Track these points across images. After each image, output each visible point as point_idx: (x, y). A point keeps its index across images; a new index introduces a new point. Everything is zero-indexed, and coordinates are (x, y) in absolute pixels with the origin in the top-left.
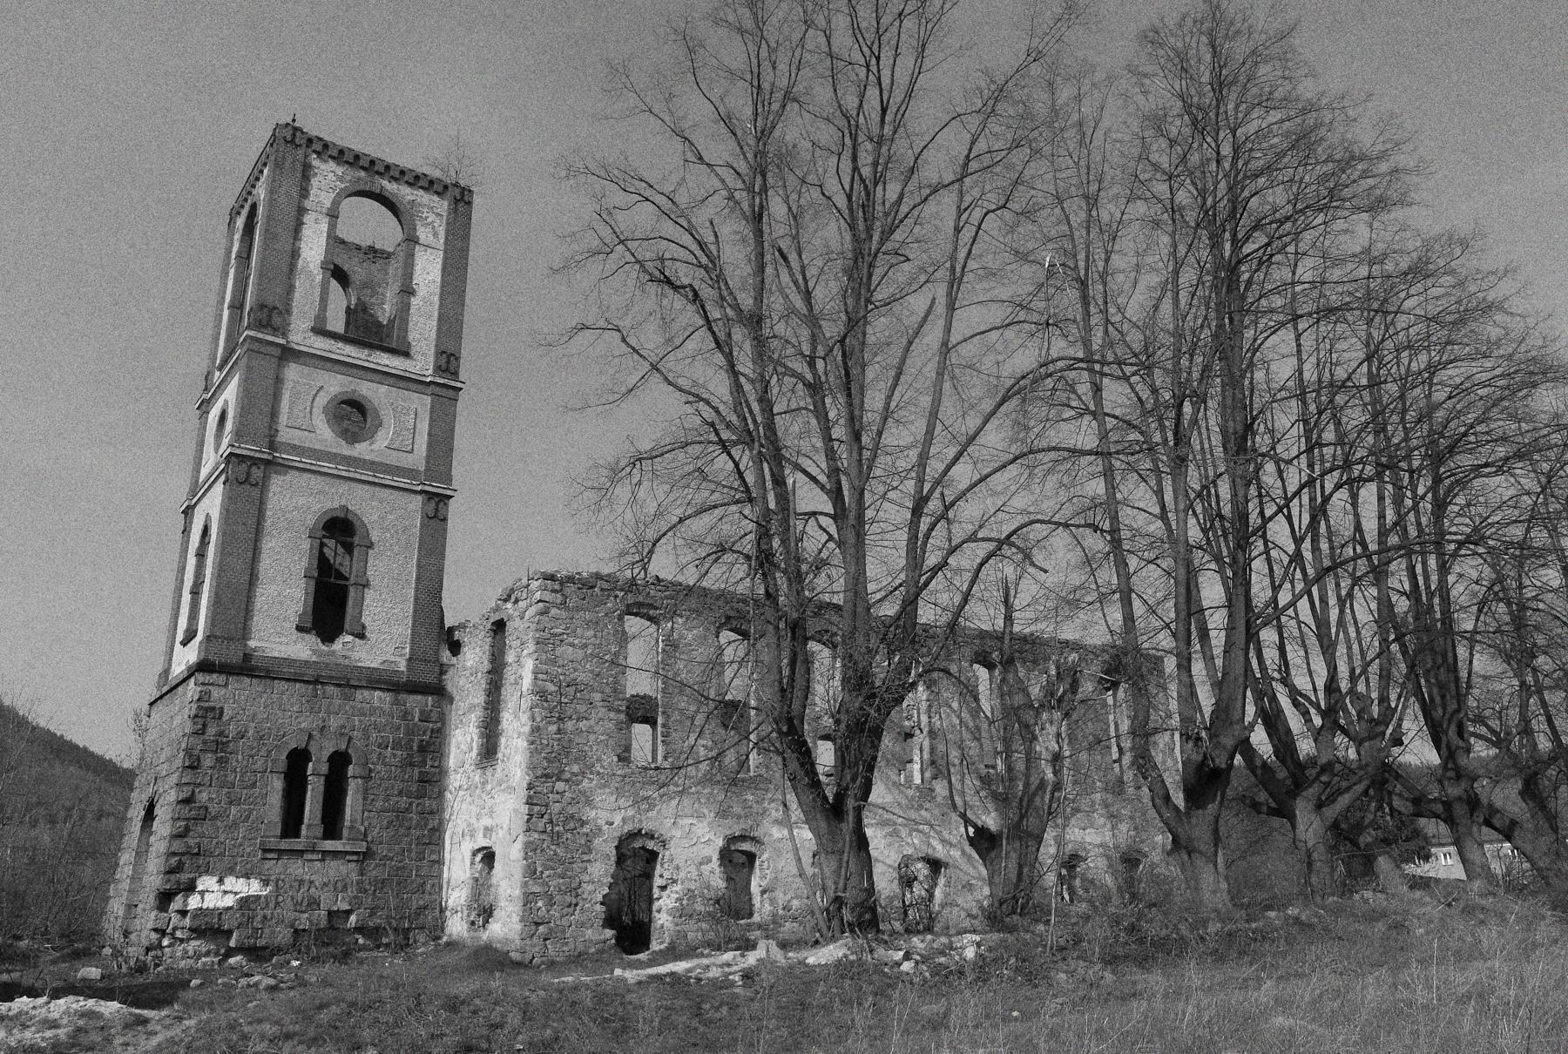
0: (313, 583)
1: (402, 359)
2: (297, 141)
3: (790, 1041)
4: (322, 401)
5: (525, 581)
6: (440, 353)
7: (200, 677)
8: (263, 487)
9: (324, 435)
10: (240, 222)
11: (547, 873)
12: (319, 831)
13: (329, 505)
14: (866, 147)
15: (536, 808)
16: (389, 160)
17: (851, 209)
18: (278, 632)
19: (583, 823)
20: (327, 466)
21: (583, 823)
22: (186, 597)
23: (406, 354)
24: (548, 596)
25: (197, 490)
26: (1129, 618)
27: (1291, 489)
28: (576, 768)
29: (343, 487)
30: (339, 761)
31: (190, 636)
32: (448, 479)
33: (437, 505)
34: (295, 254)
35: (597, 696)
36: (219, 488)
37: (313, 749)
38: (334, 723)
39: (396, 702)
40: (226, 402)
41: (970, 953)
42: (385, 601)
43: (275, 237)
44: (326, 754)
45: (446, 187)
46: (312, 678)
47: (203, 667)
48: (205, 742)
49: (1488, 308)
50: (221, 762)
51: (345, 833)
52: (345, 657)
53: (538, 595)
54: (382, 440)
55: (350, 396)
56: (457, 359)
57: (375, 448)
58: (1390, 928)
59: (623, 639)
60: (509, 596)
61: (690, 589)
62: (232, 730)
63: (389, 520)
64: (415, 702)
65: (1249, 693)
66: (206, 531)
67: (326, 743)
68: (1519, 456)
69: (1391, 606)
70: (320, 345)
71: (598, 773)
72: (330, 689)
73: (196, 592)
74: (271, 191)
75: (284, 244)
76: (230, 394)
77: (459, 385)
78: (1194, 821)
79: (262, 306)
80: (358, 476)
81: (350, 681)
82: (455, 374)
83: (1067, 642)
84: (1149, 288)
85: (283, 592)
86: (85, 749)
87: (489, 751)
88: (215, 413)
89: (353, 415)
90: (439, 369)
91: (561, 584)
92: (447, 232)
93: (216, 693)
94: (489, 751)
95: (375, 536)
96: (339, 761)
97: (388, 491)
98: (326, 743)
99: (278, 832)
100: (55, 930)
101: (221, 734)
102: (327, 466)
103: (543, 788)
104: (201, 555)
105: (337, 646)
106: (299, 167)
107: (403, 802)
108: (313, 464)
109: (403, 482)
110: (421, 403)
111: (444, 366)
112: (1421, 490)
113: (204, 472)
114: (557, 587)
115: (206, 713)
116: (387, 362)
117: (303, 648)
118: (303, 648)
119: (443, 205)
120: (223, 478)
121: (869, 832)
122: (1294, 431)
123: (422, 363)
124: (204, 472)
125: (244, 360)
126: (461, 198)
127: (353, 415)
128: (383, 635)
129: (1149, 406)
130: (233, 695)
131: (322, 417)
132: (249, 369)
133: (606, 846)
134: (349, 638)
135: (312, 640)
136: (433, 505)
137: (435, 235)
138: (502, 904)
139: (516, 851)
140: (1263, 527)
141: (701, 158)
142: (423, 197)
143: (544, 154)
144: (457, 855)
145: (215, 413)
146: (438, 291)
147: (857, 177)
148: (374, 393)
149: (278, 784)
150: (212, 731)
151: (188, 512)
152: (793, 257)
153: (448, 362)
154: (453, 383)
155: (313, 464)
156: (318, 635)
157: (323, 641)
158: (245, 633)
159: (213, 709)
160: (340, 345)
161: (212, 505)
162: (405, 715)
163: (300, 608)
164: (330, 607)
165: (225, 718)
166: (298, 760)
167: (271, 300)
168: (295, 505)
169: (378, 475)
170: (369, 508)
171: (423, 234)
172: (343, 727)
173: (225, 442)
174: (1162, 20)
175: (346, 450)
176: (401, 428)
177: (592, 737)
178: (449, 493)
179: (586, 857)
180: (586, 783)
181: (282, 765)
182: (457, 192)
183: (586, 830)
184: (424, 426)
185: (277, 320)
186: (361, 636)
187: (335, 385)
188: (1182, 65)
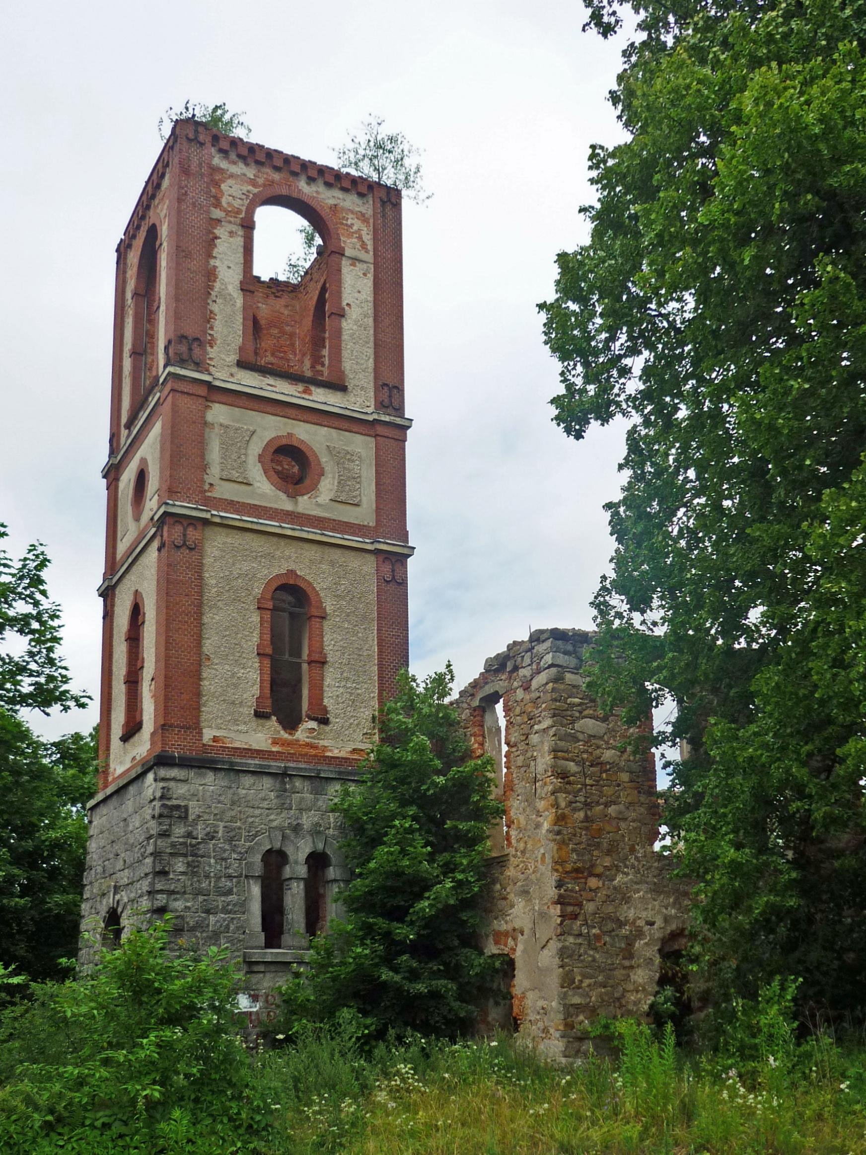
1: (339, 394)
4: (256, 448)
8: (195, 548)
9: (264, 489)
10: (134, 257)
11: (587, 982)
13: (276, 571)
15: (570, 909)
18: (233, 718)
19: (621, 924)
20: (272, 525)
21: (621, 924)
24: (562, 659)
28: (607, 862)
29: (290, 550)
31: (132, 729)
32: (404, 535)
33: (394, 563)
34: (211, 275)
35: (625, 777)
36: (152, 555)
37: (289, 850)
42: (347, 679)
43: (188, 255)
44: (302, 856)
47: (161, 761)
48: (173, 845)
49: (505, 899)
50: (193, 870)
53: (548, 659)
54: (327, 488)
55: (284, 442)
57: (319, 500)
62: (200, 831)
63: (339, 584)
65: (157, 428)
66: (136, 611)
69: (838, 857)
70: (249, 381)
71: (633, 867)
72: (298, 783)
78: (552, 844)
79: (182, 338)
80: (304, 535)
81: (321, 772)
82: (399, 410)
85: (234, 676)
88: (128, 477)
89: (292, 465)
90: (381, 405)
92: (375, 239)
93: (181, 790)
94: (290, 606)
95: (329, 605)
98: (301, 843)
100: (337, 149)
101: (189, 835)
102: (272, 525)
105: (301, 735)
108: (249, 523)
109: (354, 540)
111: (179, 542)
112: (780, 30)
114: (570, 648)
115: (171, 812)
116: (321, 399)
117: (261, 737)
118: (261, 737)
119: (367, 207)
120: (156, 544)
123: (360, 401)
125: (167, 407)
127: (292, 465)
130: (199, 790)
131: (259, 466)
132: (175, 410)
133: (647, 949)
134: (313, 724)
138: (532, 1017)
139: (548, 957)
142: (350, 201)
143: (504, 139)
145: (128, 477)
146: (371, 312)
148: (312, 436)
150: (179, 830)
153: (390, 390)
155: (249, 523)
157: (285, 728)
158: (196, 727)
159: (178, 807)
160: (271, 381)
163: (256, 691)
164: (286, 696)
166: (275, 860)
167: (191, 331)
169: (324, 535)
170: (318, 573)
171: (350, 247)
172: (318, 824)
175: (286, 504)
177: (623, 825)
178: (405, 551)
179: (627, 963)
180: (619, 878)
181: (258, 868)
182: (383, 194)
187: (270, 428)
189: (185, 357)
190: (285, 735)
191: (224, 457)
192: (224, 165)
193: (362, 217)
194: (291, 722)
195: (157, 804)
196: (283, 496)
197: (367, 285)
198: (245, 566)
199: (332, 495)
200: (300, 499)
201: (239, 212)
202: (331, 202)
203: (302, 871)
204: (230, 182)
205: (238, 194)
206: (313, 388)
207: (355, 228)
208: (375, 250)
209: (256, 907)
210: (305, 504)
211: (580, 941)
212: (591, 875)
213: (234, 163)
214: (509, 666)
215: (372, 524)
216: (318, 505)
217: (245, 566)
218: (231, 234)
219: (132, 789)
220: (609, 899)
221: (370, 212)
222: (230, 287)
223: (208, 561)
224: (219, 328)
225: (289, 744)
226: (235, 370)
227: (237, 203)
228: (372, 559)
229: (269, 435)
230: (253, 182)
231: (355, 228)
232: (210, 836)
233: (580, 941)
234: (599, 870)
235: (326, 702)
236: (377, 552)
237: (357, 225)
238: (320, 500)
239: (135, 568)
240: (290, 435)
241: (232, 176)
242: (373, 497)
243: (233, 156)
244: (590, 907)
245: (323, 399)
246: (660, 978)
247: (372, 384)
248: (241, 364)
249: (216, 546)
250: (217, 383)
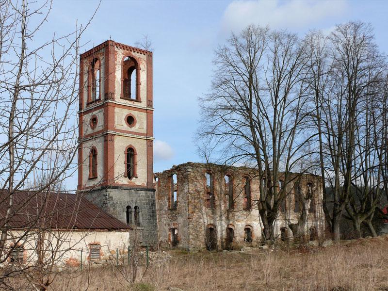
3: (159, 260)
9: (125, 126)
17: (275, 123)
19: (200, 222)
21: (200, 222)
23: (141, 102)
27: (362, 152)
33: (150, 143)
39: (146, 194)
41: (291, 216)
56: (152, 101)
57: (135, 128)
58: (264, 276)
59: (89, 258)
61: (295, 195)
63: (140, 147)
68: (11, 139)
75: (149, 79)
77: (153, 109)
81: (137, 189)
83: (264, 231)
89: (130, 120)
90: (148, 105)
94: (130, 153)
96: (136, 208)
102: (127, 135)
105: (132, 181)
107: (288, 253)
110: (144, 115)
117: (125, 181)
118: (125, 181)
122: (77, 92)
123: (143, 104)
126: (149, 55)
127: (130, 120)
129: (292, 184)
134: (135, 178)
135: (127, 179)
136: (149, 143)
137: (145, 67)
141: (69, 104)
147: (291, 154)
148: (135, 114)
149: (125, 214)
152: (90, 279)
153: (150, 103)
154: (113, 102)
157: (129, 179)
162: (148, 197)
164: (130, 173)
168: (120, 146)
174: (212, 76)
175: (129, 129)
176: (140, 125)
182: (149, 53)
183: (200, 224)
186: (137, 178)
187: (126, 113)
188: (294, 253)
190: (129, 181)
194: (130, 178)
203: (134, 210)
209: (287, 205)
210: (133, 129)
214: (178, 169)
223: (115, 143)
226: (120, 99)
228: (146, 141)
236: (147, 140)
243: (119, 48)
246: (260, 213)
250: (117, 103)
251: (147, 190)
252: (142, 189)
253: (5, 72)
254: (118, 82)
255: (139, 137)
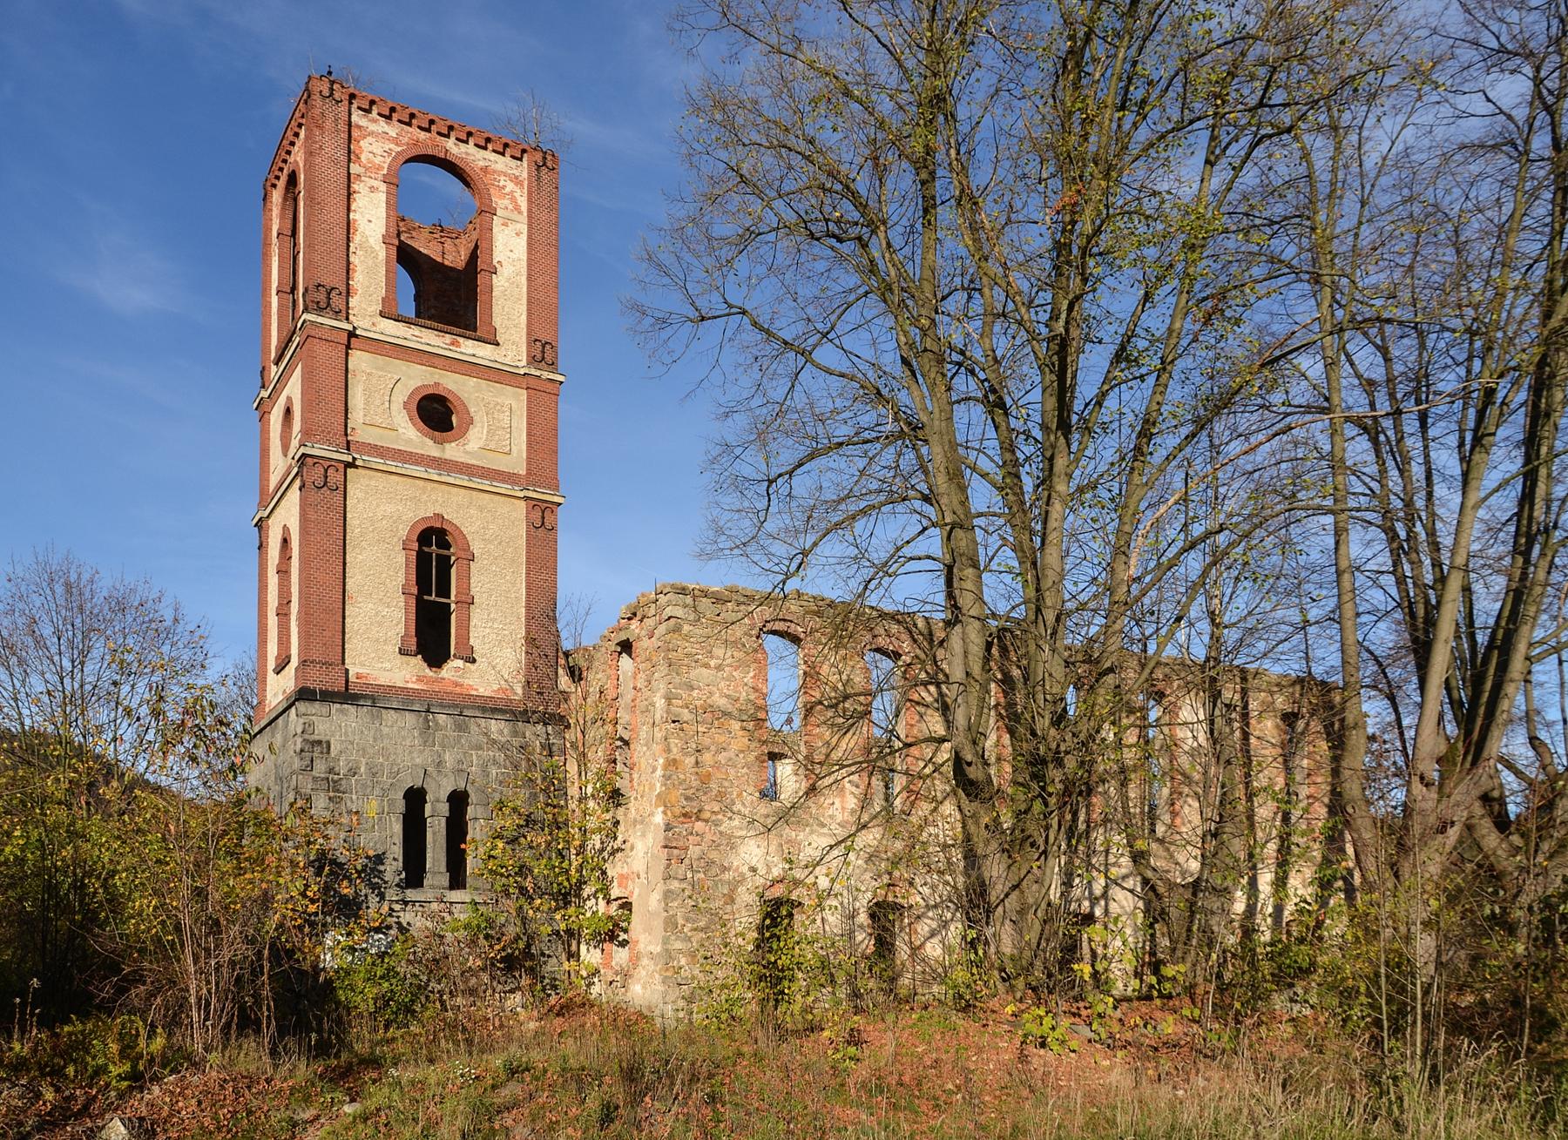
0: (413, 602)
2: (337, 96)
4: (401, 396)
5: (653, 596)
6: (532, 341)
7: (302, 706)
9: (411, 435)
12: (445, 880)
14: (1253, 440)
16: (560, 527)
19: (725, 869)
21: (725, 869)
22: (272, 621)
24: (679, 612)
25: (269, 500)
26: (1471, 344)
29: (440, 493)
30: (458, 801)
32: (555, 487)
36: (294, 495)
38: (449, 758)
39: (515, 733)
40: (289, 399)
45: (938, 52)
46: (424, 706)
47: (304, 694)
48: (315, 779)
51: (469, 880)
52: (457, 684)
57: (470, 446)
58: (1313, 964)
60: (635, 614)
64: (534, 734)
66: (285, 542)
67: (444, 782)
73: (283, 614)
74: (310, 154)
76: (293, 389)
81: (467, 708)
84: (1493, 531)
86: (417, 583)
87: (285, 542)
90: (532, 360)
91: (694, 598)
92: (530, 201)
94: (434, 557)
96: (458, 801)
97: (486, 496)
98: (444, 782)
99: (447, 884)
101: (331, 770)
102: (418, 471)
103: (681, 829)
104: (283, 572)
106: (343, 127)
109: (504, 488)
113: (274, 480)
117: (408, 673)
119: (523, 169)
120: (298, 483)
121: (1531, 753)
124: (274, 480)
127: (436, 413)
128: (493, 655)
133: (746, 897)
134: (460, 663)
139: (655, 899)
140: (1088, 832)
142: (502, 163)
144: (520, 451)
146: (524, 271)
150: (320, 768)
151: (260, 525)
156: (425, 659)
157: (430, 666)
159: (319, 742)
161: (288, 515)
163: (401, 579)
164: (433, 634)
165: (333, 752)
166: (415, 799)
168: (381, 515)
172: (460, 762)
173: (295, 443)
181: (401, 806)
182: (538, 157)
183: (727, 876)
184: (521, 424)
185: (337, 302)
187: (418, 378)
189: (323, 305)
190: (428, 672)
191: (367, 403)
192: (363, 122)
193: (516, 180)
195: (299, 740)
196: (431, 443)
197: (521, 245)
198: (390, 509)
199: (481, 444)
200: (447, 445)
201: (380, 168)
202: (482, 163)
203: (444, 808)
204: (369, 139)
205: (379, 151)
206: (461, 340)
207: (507, 190)
208: (530, 211)
210: (452, 451)
211: (684, 885)
212: (698, 819)
213: (375, 121)
215: (523, 472)
216: (467, 453)
217: (390, 509)
218: (373, 189)
219: (280, 720)
220: (715, 845)
221: (525, 175)
222: (371, 241)
224: (358, 280)
225: (436, 680)
227: (378, 160)
228: (523, 504)
229: (414, 384)
230: (396, 141)
231: (507, 190)
232: (353, 772)
233: (684, 885)
234: (706, 815)
235: (472, 642)
236: (527, 498)
237: (510, 186)
238: (470, 447)
239: (283, 503)
240: (437, 384)
241: (371, 134)
242: (524, 447)
244: (694, 851)
245: (471, 351)
247: (524, 339)
248: (382, 314)
249: (360, 486)
251: (519, 715)
252: (494, 710)
253: (763, 613)
254: (370, 251)
255: (477, 483)
